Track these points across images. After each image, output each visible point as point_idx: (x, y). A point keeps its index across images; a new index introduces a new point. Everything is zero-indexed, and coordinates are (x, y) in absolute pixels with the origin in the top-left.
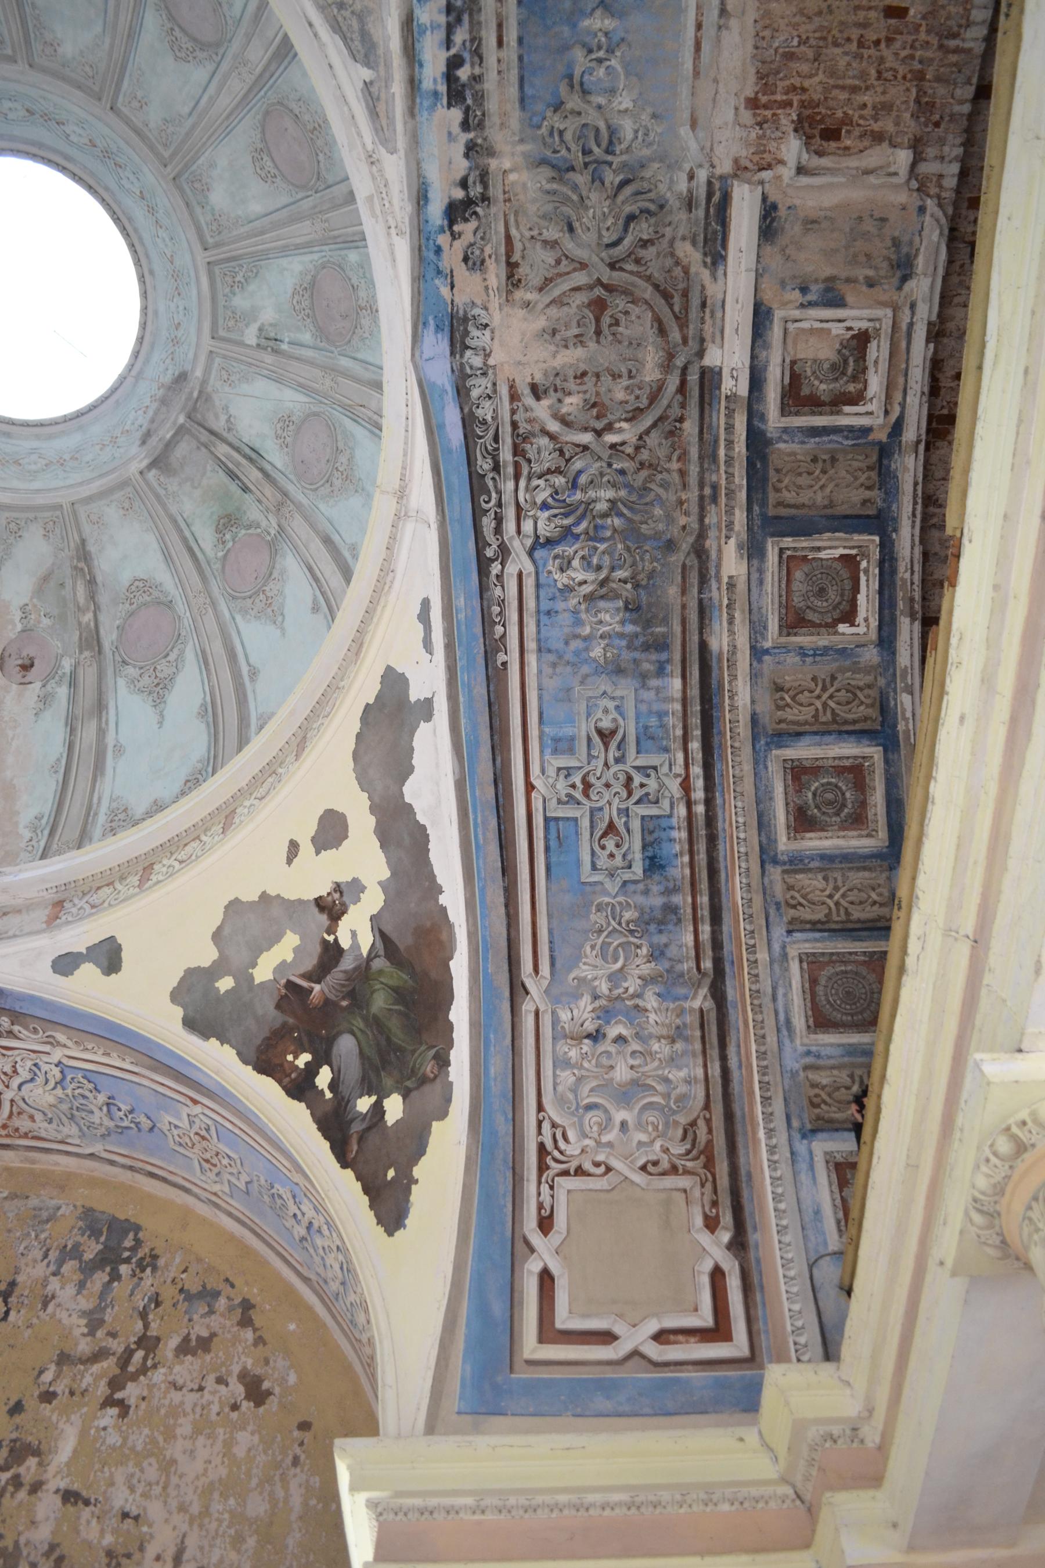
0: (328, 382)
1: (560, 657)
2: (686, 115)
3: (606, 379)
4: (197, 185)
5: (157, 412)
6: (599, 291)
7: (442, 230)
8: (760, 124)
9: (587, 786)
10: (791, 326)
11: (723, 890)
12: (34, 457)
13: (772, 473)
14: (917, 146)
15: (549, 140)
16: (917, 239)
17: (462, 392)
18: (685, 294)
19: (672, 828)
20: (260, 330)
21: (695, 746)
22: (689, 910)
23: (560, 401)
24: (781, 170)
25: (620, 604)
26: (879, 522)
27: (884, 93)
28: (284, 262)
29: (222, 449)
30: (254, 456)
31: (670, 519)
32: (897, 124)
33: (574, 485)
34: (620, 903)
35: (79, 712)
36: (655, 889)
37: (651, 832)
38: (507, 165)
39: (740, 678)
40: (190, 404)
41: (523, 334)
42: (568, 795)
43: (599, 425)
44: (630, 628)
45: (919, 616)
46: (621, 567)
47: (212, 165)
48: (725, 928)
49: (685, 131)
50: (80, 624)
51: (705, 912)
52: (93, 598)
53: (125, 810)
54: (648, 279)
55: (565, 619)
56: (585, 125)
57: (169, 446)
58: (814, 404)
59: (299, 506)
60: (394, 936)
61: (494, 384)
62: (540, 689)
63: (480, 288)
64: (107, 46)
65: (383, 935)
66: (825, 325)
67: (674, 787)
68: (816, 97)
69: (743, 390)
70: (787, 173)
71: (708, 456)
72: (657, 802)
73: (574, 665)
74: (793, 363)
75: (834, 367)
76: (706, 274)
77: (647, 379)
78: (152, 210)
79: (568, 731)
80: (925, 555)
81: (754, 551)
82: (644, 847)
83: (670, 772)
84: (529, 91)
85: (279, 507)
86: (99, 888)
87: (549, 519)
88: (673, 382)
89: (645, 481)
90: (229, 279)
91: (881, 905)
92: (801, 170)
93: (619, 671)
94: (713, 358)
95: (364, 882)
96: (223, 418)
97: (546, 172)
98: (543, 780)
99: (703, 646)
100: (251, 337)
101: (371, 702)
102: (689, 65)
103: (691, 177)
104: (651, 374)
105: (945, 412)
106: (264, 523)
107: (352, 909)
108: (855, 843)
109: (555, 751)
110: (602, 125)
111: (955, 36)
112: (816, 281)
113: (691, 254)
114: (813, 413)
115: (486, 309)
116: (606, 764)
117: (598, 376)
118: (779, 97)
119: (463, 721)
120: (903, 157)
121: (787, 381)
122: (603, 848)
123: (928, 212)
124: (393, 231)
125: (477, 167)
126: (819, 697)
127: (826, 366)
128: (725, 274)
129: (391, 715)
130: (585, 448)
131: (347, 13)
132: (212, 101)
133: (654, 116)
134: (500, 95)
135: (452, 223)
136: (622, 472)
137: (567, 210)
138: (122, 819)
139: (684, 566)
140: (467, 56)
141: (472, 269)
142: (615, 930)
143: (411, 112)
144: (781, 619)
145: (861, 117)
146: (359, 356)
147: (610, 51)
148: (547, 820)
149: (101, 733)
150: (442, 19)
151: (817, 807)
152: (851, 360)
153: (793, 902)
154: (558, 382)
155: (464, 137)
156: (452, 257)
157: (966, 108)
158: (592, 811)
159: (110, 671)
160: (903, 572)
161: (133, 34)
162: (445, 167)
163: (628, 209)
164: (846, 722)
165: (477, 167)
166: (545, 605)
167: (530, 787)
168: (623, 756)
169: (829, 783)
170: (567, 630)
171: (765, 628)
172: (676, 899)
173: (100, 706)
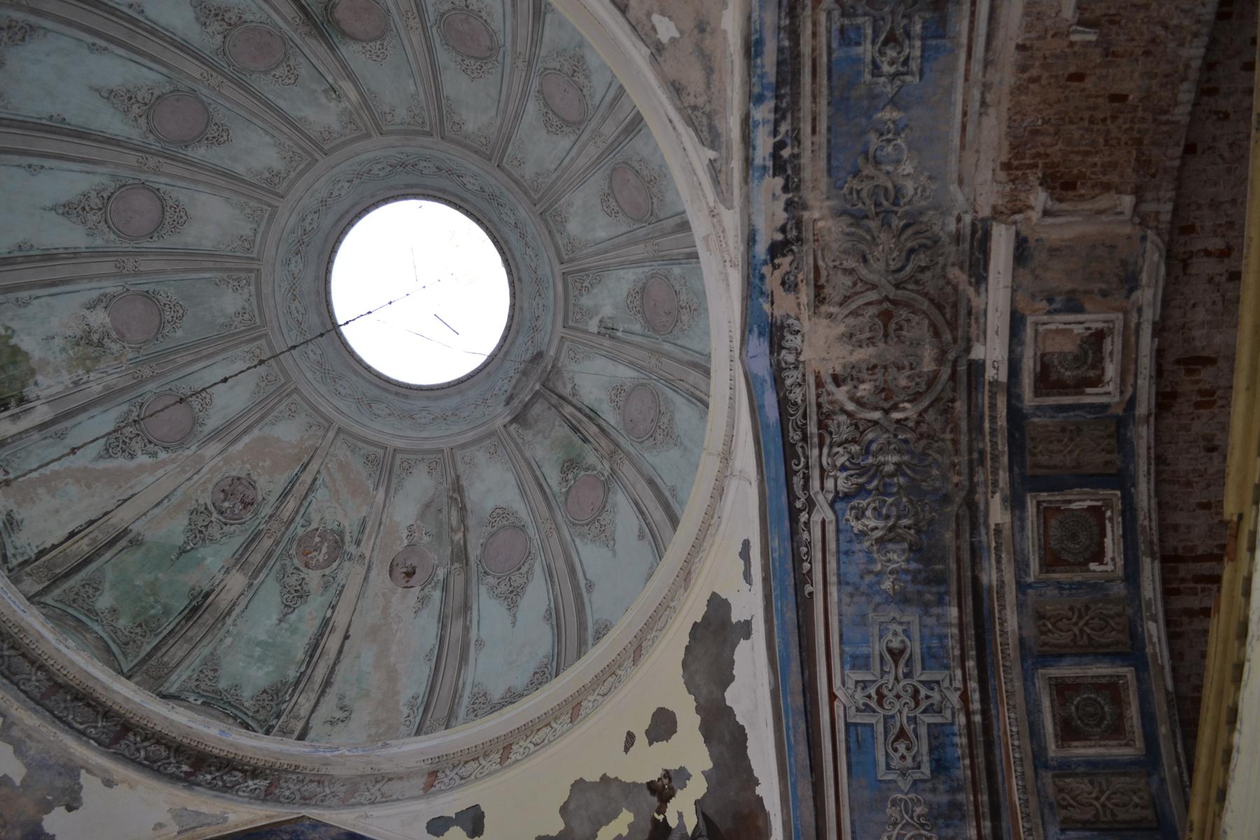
0: (653, 362)
1: (857, 589)
2: (955, 176)
3: (892, 371)
4: (558, 218)
5: (518, 381)
6: (886, 305)
7: (765, 263)
8: (1013, 181)
9: (881, 697)
10: (1041, 328)
11: (1001, 791)
12: (424, 413)
13: (1028, 441)
14: (1138, 192)
15: (849, 197)
16: (1141, 260)
17: (778, 381)
18: (955, 306)
19: (954, 735)
20: (601, 321)
21: (971, 664)
22: (972, 808)
23: (855, 387)
24: (1030, 213)
25: (906, 546)
26: (1122, 480)
27: (1110, 155)
28: (622, 273)
29: (568, 410)
30: (593, 415)
31: (945, 478)
32: (1122, 176)
33: (867, 451)
34: (912, 800)
35: (449, 611)
36: (942, 787)
37: (936, 738)
38: (816, 215)
39: (1008, 608)
40: (545, 375)
41: (827, 338)
42: (865, 704)
43: (887, 405)
44: (913, 566)
45: (1158, 555)
46: (905, 516)
47: (570, 204)
48: (1004, 824)
49: (954, 188)
50: (452, 541)
51: (986, 810)
52: (463, 521)
53: (485, 695)
54: (926, 295)
55: (860, 558)
56: (877, 186)
57: (527, 406)
58: (1061, 387)
59: (628, 455)
60: (716, 820)
61: (804, 375)
62: (840, 615)
63: (794, 305)
64: (498, 124)
65: (704, 815)
66: (1068, 327)
67: (955, 698)
68: (1056, 160)
69: (1003, 377)
70: (1035, 215)
71: (975, 428)
72: (940, 712)
73: (868, 595)
74: (1043, 355)
75: (1076, 358)
76: (971, 291)
77: (925, 370)
78: (522, 236)
79: (864, 650)
80: (1159, 504)
81: (1015, 503)
82: (931, 750)
83: (951, 685)
84: (834, 163)
85: (612, 455)
86: (466, 762)
87: (847, 478)
88: (946, 373)
89: (924, 449)
90: (578, 285)
91: (1143, 808)
92: (1046, 213)
93: (903, 599)
94: (978, 353)
95: (690, 771)
96: (569, 386)
97: (846, 219)
98: (842, 692)
99: (976, 581)
100: (593, 326)
101: (699, 620)
102: (957, 141)
103: (959, 219)
104: (928, 366)
105: (1168, 389)
106: (599, 467)
107: (679, 793)
108: (1115, 751)
109: (853, 667)
110: (890, 186)
111: (1166, 112)
112: (1060, 293)
113: (958, 275)
114: (1061, 394)
115: (798, 319)
116: (896, 679)
117: (885, 368)
118: (1027, 161)
119: (777, 641)
120: (1128, 201)
121: (1038, 369)
122: (896, 750)
123: (1149, 240)
124: (728, 264)
125: (793, 218)
126: (1076, 624)
127: (1070, 357)
128: (987, 290)
129: (715, 633)
130: (876, 423)
131: (699, 114)
132: (573, 160)
133: (930, 178)
134: (813, 167)
135: (773, 257)
136: (906, 441)
137: (863, 247)
138: (484, 705)
139: (957, 516)
140: (789, 141)
141: (788, 290)
142: (908, 823)
143: (746, 180)
144: (1040, 559)
145: (1093, 173)
146: (679, 342)
147: (897, 134)
148: (847, 725)
149: (466, 629)
150: (772, 116)
151: (1080, 718)
152: (1090, 353)
153: (1065, 803)
154: (854, 373)
155: (784, 197)
156: (773, 281)
157: (1177, 163)
158: (886, 718)
159: (474, 580)
160: (1142, 520)
161: (518, 117)
162: (770, 217)
163: (909, 245)
164: (1101, 645)
165: (793, 218)
166: (843, 547)
167: (832, 697)
168: (911, 672)
169: (1089, 698)
170: (862, 567)
171: (1028, 566)
172: (961, 797)
173: (466, 608)
